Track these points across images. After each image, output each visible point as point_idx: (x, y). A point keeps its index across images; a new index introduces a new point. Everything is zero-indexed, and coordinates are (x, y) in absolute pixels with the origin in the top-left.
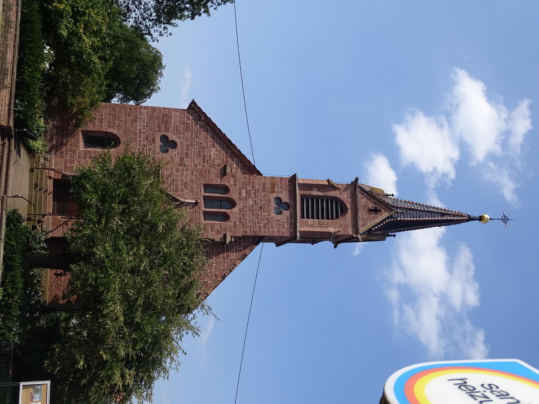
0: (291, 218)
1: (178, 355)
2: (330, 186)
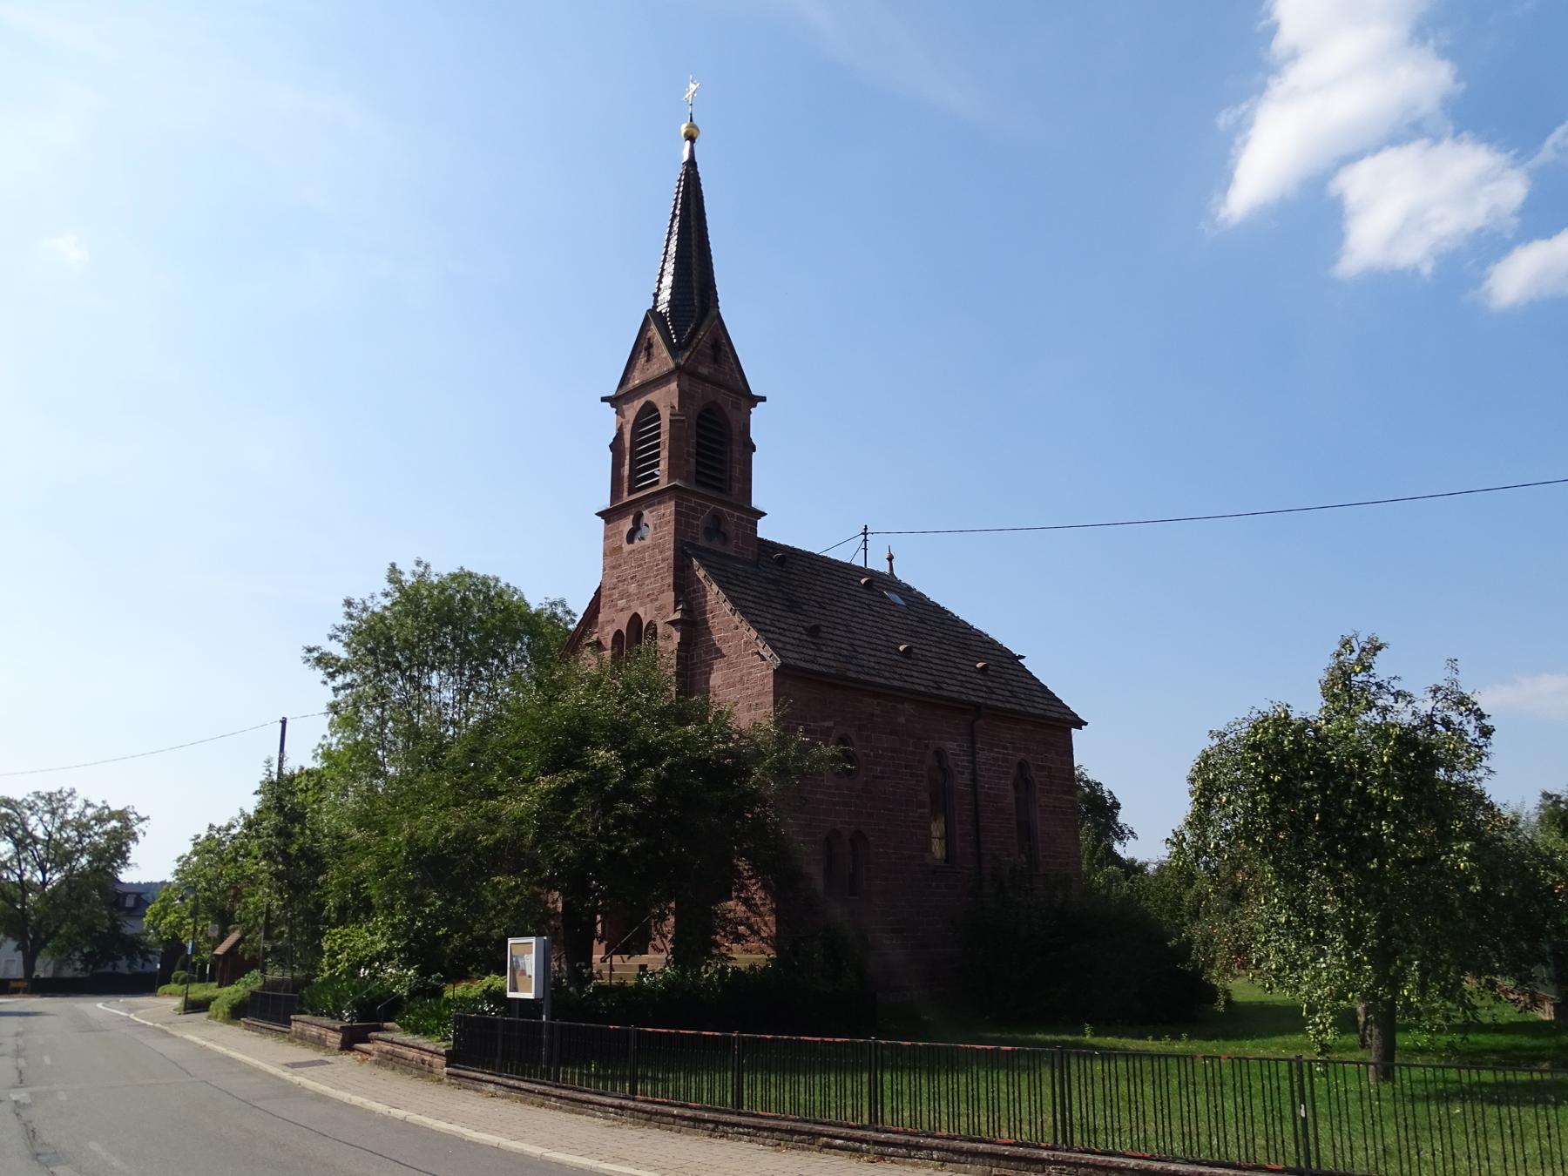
0: (651, 506)
1: (1448, 673)
2: (616, 446)
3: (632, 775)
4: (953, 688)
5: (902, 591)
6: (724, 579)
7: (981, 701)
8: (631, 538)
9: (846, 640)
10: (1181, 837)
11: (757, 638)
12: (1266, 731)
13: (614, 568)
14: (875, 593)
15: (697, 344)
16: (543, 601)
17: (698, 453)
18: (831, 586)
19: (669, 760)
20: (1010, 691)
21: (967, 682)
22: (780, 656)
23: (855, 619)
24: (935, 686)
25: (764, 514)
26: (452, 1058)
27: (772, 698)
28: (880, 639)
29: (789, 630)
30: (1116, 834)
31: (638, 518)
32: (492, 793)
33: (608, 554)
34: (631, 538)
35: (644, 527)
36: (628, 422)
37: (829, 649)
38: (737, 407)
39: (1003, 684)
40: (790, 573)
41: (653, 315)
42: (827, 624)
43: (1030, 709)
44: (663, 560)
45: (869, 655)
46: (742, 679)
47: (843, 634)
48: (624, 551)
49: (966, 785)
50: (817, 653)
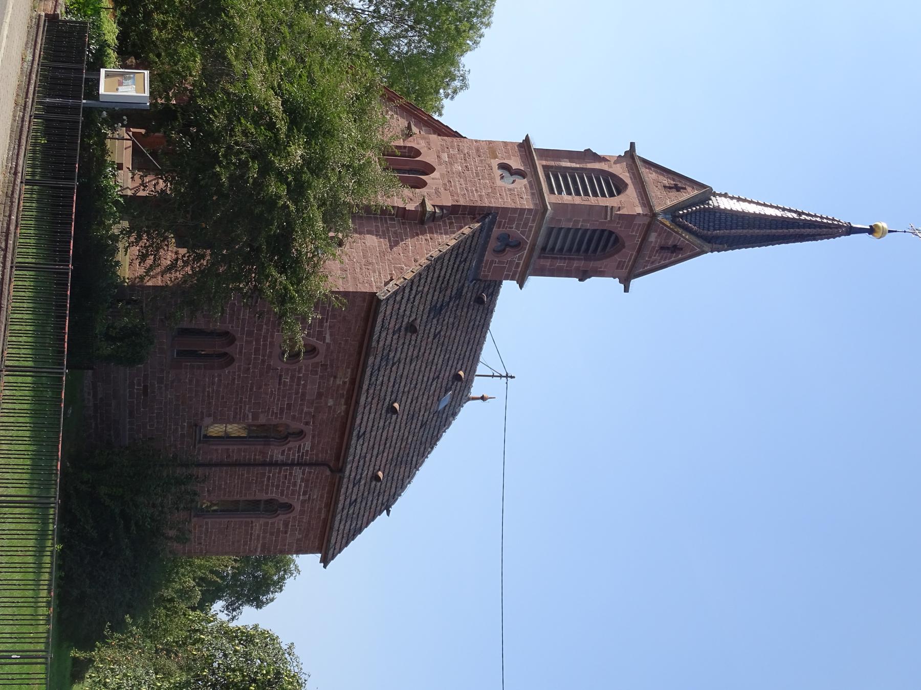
2: (588, 155)
3: (281, 176)
4: (359, 448)
5: (452, 408)
6: (461, 250)
7: (347, 473)
8: (504, 167)
9: (404, 355)
10: (212, 619)
11: (405, 279)
12: (291, 683)
13: (478, 150)
14: (450, 383)
15: (677, 232)
16: (467, 68)
17: (577, 230)
18: (456, 345)
19: (293, 208)
20: (356, 500)
21: (365, 462)
22: (388, 299)
23: (424, 365)
24: (361, 434)
25: (521, 287)
26: (52, 19)
27: (351, 290)
28: (405, 386)
29: (412, 307)
30: (232, 604)
31: (521, 174)
32: (271, 57)
33: (491, 145)
34: (504, 167)
35: (512, 179)
36: (610, 167)
37: (395, 342)
38: (620, 266)
39: (363, 495)
40: (468, 308)
41: (707, 193)
42: (419, 339)
43: (338, 518)
44: (480, 196)
45: (390, 377)
46: (370, 263)
47: (410, 354)
48: (492, 160)
49: (272, 456)
50: (391, 331)
